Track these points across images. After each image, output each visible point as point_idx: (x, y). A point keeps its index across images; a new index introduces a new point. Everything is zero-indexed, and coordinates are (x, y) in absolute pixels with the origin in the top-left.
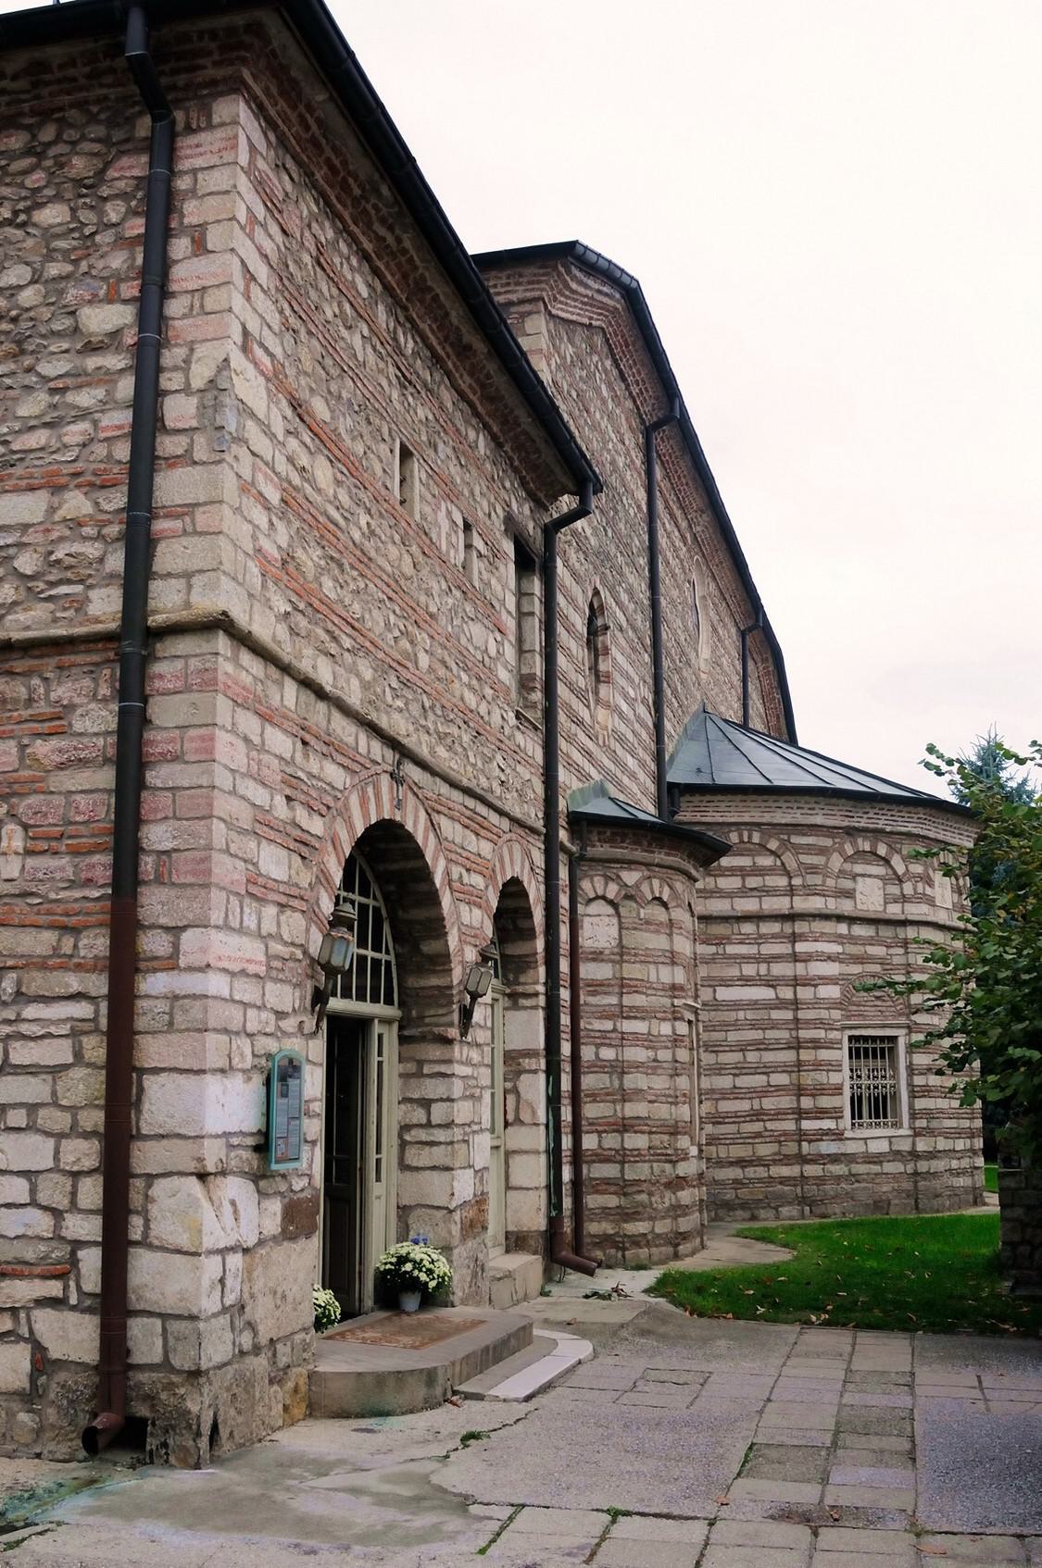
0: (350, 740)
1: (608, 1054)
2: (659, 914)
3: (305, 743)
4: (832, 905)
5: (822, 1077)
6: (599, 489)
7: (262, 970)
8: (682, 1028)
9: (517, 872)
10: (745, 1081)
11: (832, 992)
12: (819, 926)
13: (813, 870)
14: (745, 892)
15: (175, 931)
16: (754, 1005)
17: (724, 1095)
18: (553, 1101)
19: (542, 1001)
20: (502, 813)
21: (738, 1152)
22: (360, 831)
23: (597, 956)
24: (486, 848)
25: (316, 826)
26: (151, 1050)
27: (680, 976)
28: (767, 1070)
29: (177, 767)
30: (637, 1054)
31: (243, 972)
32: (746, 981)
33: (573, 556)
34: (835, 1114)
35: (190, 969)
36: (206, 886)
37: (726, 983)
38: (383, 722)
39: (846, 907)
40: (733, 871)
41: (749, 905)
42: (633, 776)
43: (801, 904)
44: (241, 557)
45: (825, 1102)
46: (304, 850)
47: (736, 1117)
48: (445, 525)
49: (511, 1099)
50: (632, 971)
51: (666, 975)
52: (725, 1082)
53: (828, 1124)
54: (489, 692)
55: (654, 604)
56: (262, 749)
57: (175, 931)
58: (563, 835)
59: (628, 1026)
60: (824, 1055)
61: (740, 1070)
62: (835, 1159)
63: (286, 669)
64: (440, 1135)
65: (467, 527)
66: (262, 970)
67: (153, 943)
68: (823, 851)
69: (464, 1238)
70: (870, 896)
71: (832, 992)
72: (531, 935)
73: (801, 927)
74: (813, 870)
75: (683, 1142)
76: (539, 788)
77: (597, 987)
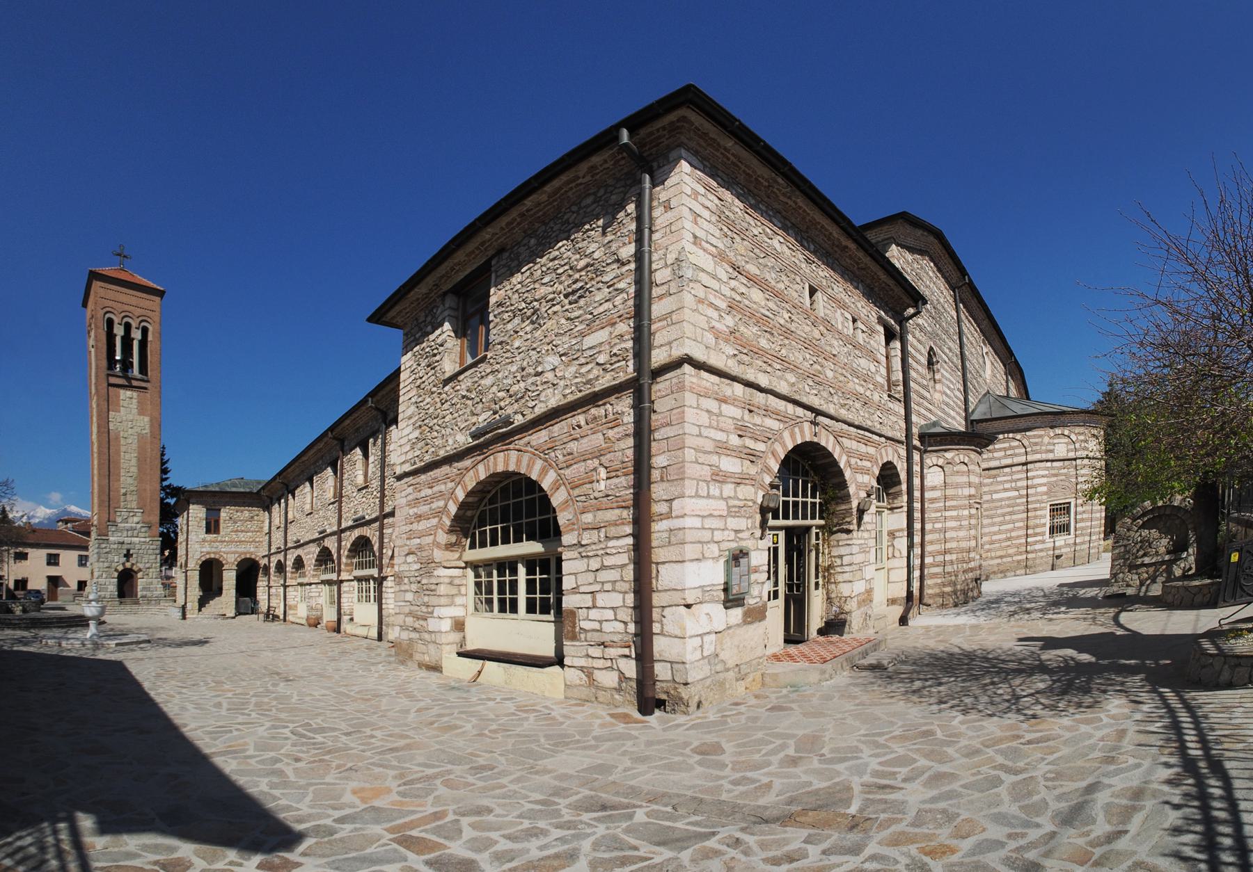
0: (782, 408)
1: (938, 526)
2: (964, 468)
3: (751, 411)
4: (1044, 456)
5: (1038, 521)
6: (925, 302)
7: (725, 513)
8: (973, 511)
9: (890, 459)
10: (1003, 527)
11: (1044, 489)
12: (1038, 465)
13: (1036, 444)
14: (1006, 456)
15: (670, 501)
16: (1009, 498)
17: (995, 534)
18: (910, 547)
19: (905, 509)
20: (880, 436)
21: (998, 553)
22: (790, 447)
23: (934, 488)
24: (871, 450)
25: (761, 447)
26: (658, 554)
27: (973, 491)
28: (1013, 522)
29: (668, 428)
30: (950, 524)
31: (711, 515)
32: (1005, 490)
33: (917, 333)
34: (1043, 534)
35: (677, 517)
36: (682, 479)
37: (996, 492)
38: (804, 400)
39: (1051, 456)
40: (1000, 450)
41: (1009, 461)
42: (954, 418)
43: (1030, 458)
44: (699, 330)
45: (1038, 530)
46: (752, 458)
47: (1000, 541)
48: (840, 319)
49: (891, 549)
50: (949, 492)
51: (966, 492)
52: (996, 529)
53: (1039, 538)
54: (871, 387)
55: (962, 353)
56: (720, 415)
57: (670, 501)
58: (916, 443)
59: (948, 514)
60: (1039, 513)
61: (1001, 524)
62: (1041, 550)
63: (734, 379)
64: (847, 569)
65: (854, 321)
66: (725, 513)
67: (658, 508)
68: (1040, 436)
69: (859, 608)
70: (1061, 450)
71: (1044, 489)
72: (899, 483)
73: (1029, 466)
74: (1036, 444)
75: (972, 555)
76: (904, 426)
77: (933, 500)
